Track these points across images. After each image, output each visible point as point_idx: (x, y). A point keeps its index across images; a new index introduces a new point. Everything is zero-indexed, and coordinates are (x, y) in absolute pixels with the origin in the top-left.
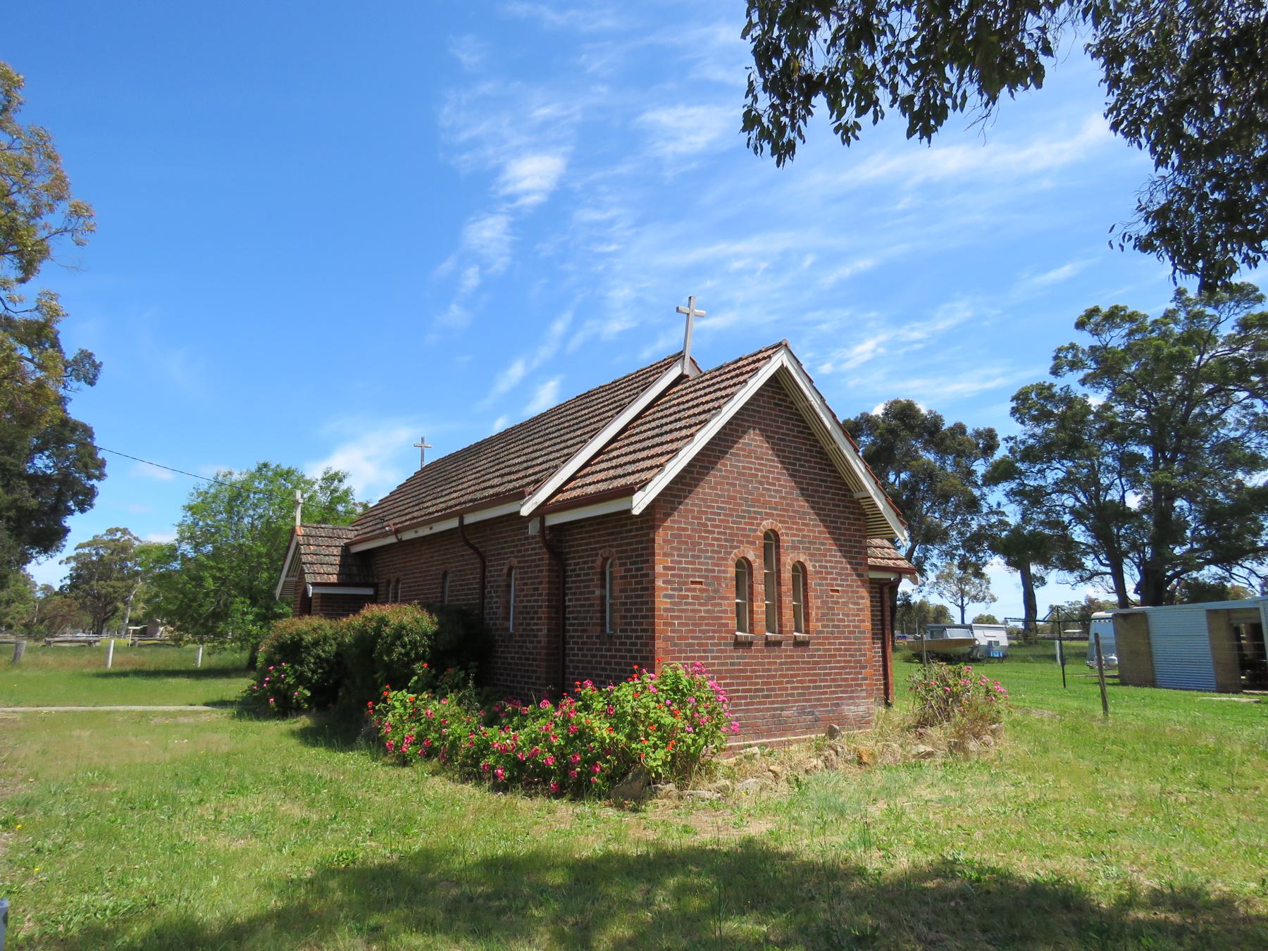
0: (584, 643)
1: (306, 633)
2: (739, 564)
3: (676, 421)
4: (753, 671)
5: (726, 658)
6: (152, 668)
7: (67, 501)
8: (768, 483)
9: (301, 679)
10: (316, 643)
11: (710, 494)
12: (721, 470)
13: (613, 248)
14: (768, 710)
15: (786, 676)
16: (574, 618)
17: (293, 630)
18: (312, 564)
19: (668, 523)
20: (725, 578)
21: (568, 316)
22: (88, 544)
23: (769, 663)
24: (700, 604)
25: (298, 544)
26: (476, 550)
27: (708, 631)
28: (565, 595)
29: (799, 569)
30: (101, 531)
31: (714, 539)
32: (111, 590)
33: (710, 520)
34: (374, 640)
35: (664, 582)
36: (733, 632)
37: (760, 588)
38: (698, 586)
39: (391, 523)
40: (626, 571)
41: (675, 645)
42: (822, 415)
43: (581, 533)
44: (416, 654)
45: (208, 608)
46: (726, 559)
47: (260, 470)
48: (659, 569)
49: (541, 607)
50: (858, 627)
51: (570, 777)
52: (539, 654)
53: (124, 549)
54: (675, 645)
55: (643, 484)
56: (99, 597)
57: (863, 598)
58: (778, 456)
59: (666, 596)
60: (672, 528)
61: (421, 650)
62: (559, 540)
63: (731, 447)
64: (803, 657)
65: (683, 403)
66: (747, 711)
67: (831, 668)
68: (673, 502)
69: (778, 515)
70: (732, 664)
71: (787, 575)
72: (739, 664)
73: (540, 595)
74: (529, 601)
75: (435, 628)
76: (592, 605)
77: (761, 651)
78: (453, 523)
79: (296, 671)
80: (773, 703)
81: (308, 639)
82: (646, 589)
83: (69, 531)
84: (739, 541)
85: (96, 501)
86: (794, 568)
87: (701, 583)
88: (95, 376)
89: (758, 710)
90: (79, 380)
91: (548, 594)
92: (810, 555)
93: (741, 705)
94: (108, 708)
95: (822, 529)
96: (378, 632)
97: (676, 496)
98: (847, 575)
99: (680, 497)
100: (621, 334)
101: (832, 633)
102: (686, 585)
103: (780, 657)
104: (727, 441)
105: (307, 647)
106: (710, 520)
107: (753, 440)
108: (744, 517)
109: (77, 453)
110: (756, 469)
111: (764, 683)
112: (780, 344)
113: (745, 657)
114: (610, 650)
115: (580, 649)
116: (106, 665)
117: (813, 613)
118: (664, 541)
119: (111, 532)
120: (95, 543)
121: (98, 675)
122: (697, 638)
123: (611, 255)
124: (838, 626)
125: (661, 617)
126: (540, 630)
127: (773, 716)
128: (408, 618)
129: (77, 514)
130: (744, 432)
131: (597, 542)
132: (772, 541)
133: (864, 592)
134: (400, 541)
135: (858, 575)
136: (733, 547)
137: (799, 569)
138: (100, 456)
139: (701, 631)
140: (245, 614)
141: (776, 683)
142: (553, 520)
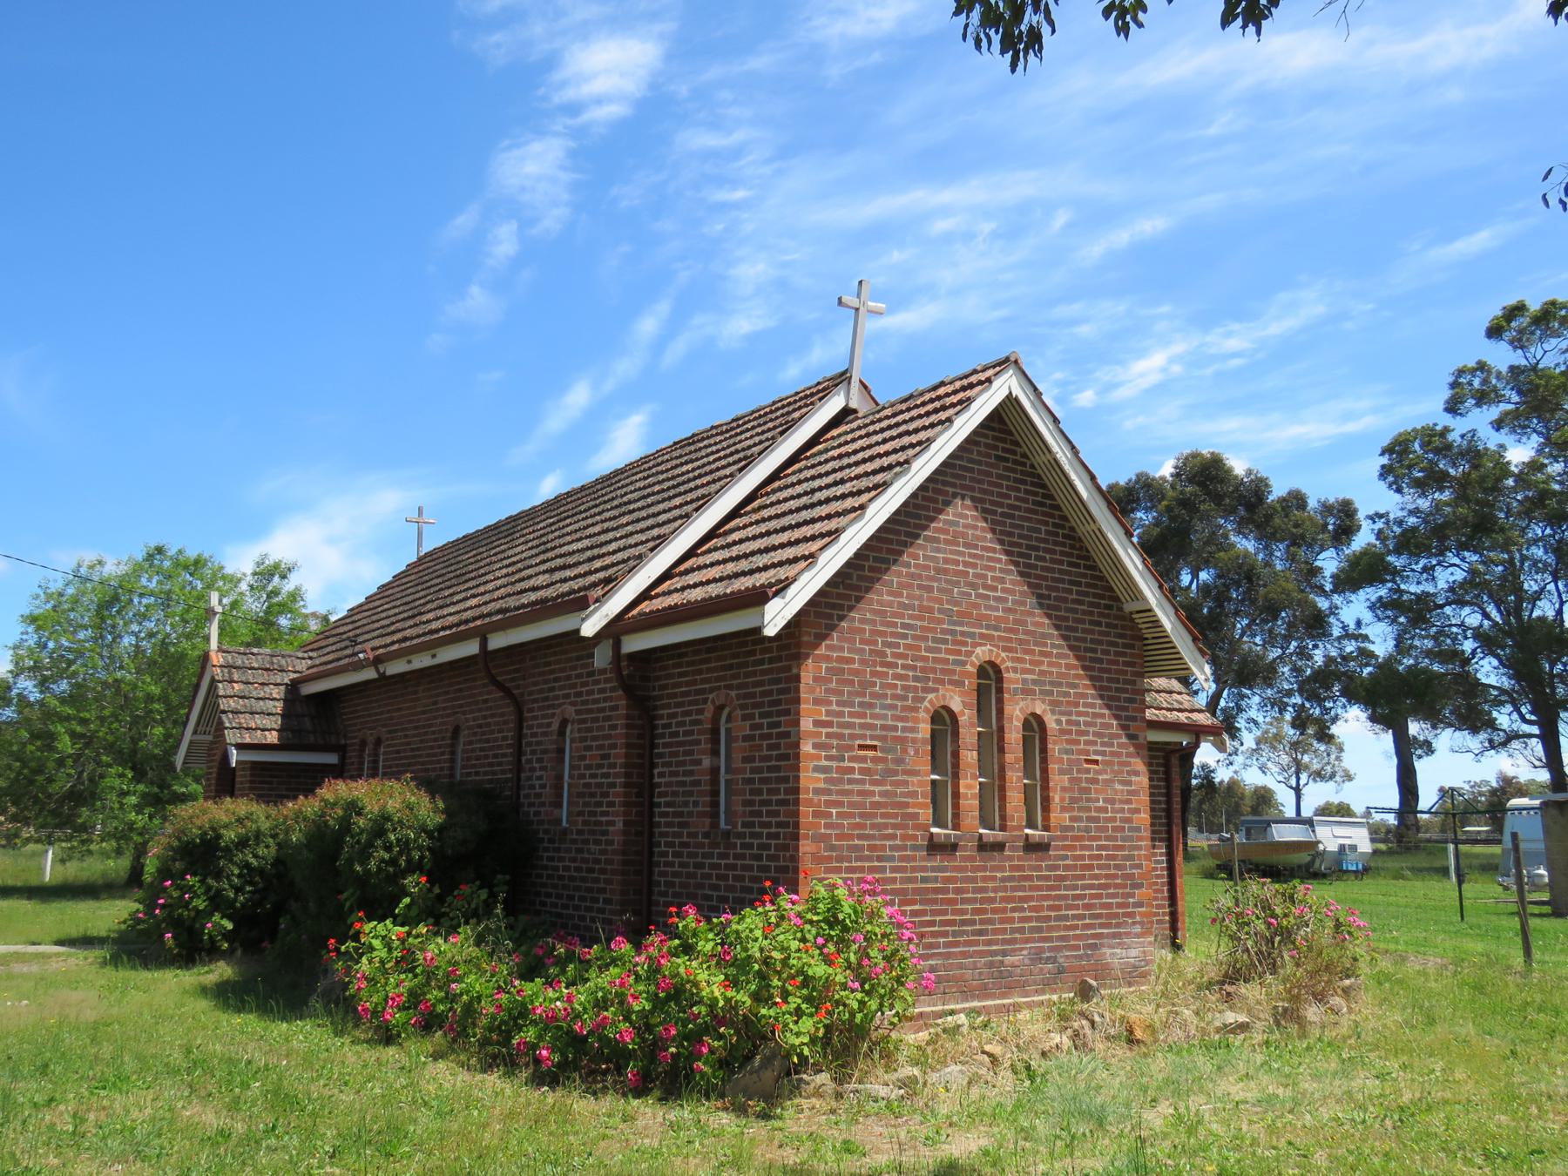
1: (226, 826)
2: (936, 718)
3: (836, 484)
4: (958, 891)
5: (914, 869)
8: (986, 587)
9: (217, 902)
10: (242, 843)
11: (890, 604)
12: (908, 565)
13: (740, 194)
14: (981, 954)
17: (204, 821)
19: (822, 650)
20: (914, 741)
21: (664, 307)
23: (985, 879)
25: (213, 681)
26: (508, 692)
27: (886, 826)
28: (653, 766)
29: (1035, 727)
31: (897, 677)
33: (890, 645)
35: (815, 746)
36: (926, 828)
37: (970, 757)
38: (870, 753)
41: (833, 848)
42: (1073, 476)
43: (679, 665)
44: (409, 861)
46: (916, 709)
47: (150, 557)
48: (806, 724)
49: (613, 785)
54: (833, 848)
57: (1136, 773)
59: (817, 769)
60: (828, 659)
61: (416, 855)
63: (925, 528)
64: (1039, 868)
65: (848, 454)
66: (948, 956)
67: (1084, 887)
68: (830, 617)
70: (924, 880)
71: (1014, 735)
72: (936, 879)
76: (697, 783)
77: (972, 859)
78: (471, 648)
79: (209, 888)
80: (990, 943)
81: (230, 835)
82: (785, 757)
86: (1027, 725)
87: (874, 748)
89: (965, 955)
97: (834, 606)
98: (1113, 736)
99: (841, 607)
100: (754, 338)
101: (1087, 830)
102: (849, 751)
103: (1002, 869)
105: (227, 849)
106: (890, 645)
107: (961, 515)
108: (945, 642)
110: (966, 564)
111: (976, 911)
112: (1007, 360)
113: (945, 869)
117: (1056, 798)
118: (816, 679)
124: (1097, 820)
125: (810, 803)
127: (991, 965)
128: (395, 802)
130: (947, 503)
132: (990, 681)
133: (1139, 765)
135: (1131, 737)
136: (927, 690)
137: (1035, 727)
139: (873, 826)
140: (123, 794)
141: (994, 911)
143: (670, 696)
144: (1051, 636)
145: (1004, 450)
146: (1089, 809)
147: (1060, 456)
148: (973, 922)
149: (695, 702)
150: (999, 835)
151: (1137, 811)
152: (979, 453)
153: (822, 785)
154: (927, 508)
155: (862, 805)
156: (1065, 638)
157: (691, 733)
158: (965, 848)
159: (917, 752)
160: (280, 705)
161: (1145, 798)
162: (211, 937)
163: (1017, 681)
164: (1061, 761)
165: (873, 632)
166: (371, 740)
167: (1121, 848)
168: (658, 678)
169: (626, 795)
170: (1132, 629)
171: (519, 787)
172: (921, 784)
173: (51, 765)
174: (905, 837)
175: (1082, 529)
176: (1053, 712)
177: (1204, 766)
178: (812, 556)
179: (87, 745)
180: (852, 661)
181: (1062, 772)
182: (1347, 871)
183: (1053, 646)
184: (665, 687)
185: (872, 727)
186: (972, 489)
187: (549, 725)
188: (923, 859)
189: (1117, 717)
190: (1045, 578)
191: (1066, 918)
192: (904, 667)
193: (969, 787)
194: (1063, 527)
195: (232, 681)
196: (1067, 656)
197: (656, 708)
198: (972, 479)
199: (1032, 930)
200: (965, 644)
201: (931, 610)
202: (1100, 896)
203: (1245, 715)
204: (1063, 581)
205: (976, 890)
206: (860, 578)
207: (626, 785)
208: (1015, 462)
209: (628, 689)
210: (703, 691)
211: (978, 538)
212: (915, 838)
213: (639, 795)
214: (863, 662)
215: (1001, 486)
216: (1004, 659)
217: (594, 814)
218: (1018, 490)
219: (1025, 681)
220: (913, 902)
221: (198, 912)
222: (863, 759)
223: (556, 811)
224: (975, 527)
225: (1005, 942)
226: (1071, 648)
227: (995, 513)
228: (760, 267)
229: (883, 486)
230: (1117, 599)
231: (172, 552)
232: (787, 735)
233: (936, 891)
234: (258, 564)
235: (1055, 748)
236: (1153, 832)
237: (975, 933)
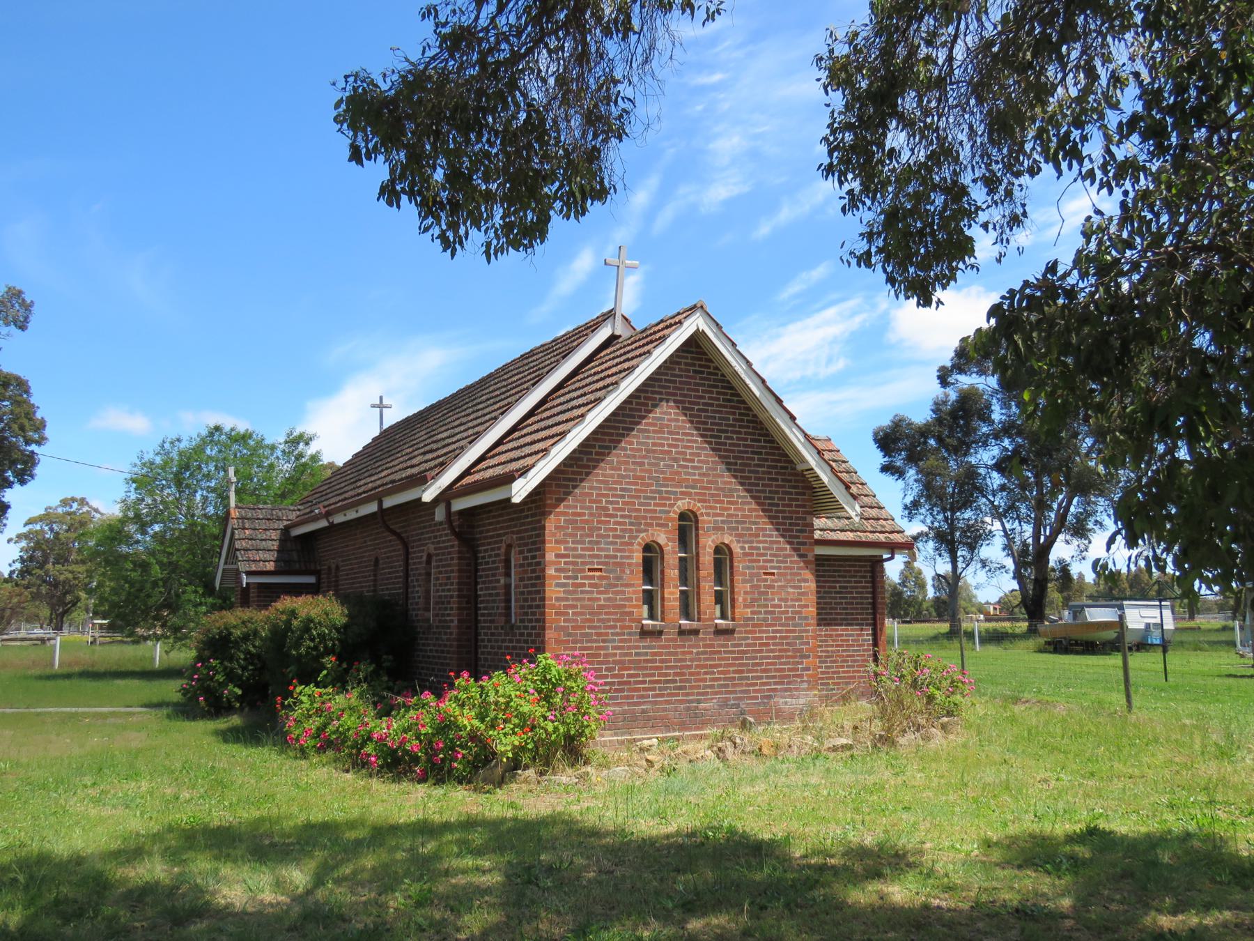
0: (492, 634)
1: (235, 627)
2: (647, 548)
3: (582, 396)
4: (662, 661)
5: (629, 647)
6: (102, 670)
7: (5, 471)
8: (685, 460)
9: (231, 677)
10: (245, 638)
11: (612, 476)
12: (625, 449)
13: (717, 77)
14: (681, 702)
15: (705, 666)
16: (485, 608)
17: (220, 624)
18: (246, 550)
19: (561, 509)
20: (630, 564)
21: (653, 182)
22: (40, 519)
23: (683, 653)
24: (599, 593)
25: (233, 529)
26: (398, 535)
27: (609, 620)
28: (476, 583)
29: (723, 556)
30: (54, 502)
31: (616, 523)
32: (70, 576)
33: (611, 502)
34: (284, 636)
35: (557, 570)
36: (639, 620)
37: (673, 573)
38: (597, 574)
39: (321, 505)
40: (525, 558)
41: (569, 635)
42: (748, 381)
43: (488, 518)
44: (326, 647)
45: (158, 597)
46: (632, 544)
47: (211, 434)
48: (550, 556)
49: (452, 597)
50: (800, 613)
51: (435, 763)
52: (451, 646)
53: (83, 524)
54: (569, 635)
55: (524, 471)
56: (55, 584)
57: (806, 581)
58: (697, 429)
59: (558, 585)
60: (565, 514)
61: (330, 644)
62: (468, 527)
63: (639, 423)
64: (727, 646)
65: (598, 373)
66: (655, 703)
67: (762, 658)
68: (567, 487)
69: (697, 494)
70: (637, 654)
71: (707, 558)
72: (646, 654)
73: (452, 584)
74: (443, 591)
75: (344, 620)
76: (498, 595)
77: (674, 640)
78: (372, 508)
79: (226, 668)
80: (687, 694)
81: (237, 633)
82: (538, 578)
83: (9, 507)
84: (646, 524)
85: (38, 470)
86: (718, 550)
87: (600, 570)
88: (26, 318)
89: (668, 702)
90: (7, 324)
91: (459, 584)
92: (737, 535)
93: (648, 696)
94: (39, 710)
95: (754, 506)
96: (288, 623)
97: (569, 480)
98: (786, 556)
99: (575, 480)
100: (729, 203)
101: (765, 619)
102: (580, 572)
103: (698, 646)
104: (633, 416)
105: (236, 642)
106: (611, 502)
107: (666, 413)
108: (654, 498)
109: (12, 412)
110: (669, 445)
111: (676, 674)
112: (695, 306)
113: (654, 647)
114: (511, 641)
115: (489, 641)
116: (53, 665)
117: (740, 599)
118: (557, 528)
119: (65, 502)
120: (48, 517)
121: (40, 678)
122: (595, 628)
123: (715, 88)
124: (772, 613)
125: (553, 606)
126: (452, 621)
127: (688, 709)
128: (324, 610)
129: (17, 486)
130: (655, 406)
131: (502, 528)
132: (687, 527)
133: (808, 575)
134: (332, 526)
135: (800, 556)
136: (639, 531)
137: (723, 556)
138: (39, 415)
139: (599, 620)
140: (197, 605)
141: (691, 674)
142: (459, 505)
143: (486, 538)
144: (737, 490)
145: (700, 366)
146: (766, 606)
147: (738, 368)
148: (675, 681)
149: (496, 542)
150: (695, 624)
151: (807, 606)
152: (680, 370)
153: (562, 595)
154: (640, 410)
155: (591, 607)
156: (747, 491)
157: (494, 562)
158: (668, 633)
159: (632, 572)
160: (276, 544)
161: (813, 597)
162: (228, 700)
163: (709, 522)
164: (745, 574)
165: (598, 495)
166: (333, 566)
167: (794, 631)
168: (479, 526)
169: (459, 603)
170: (803, 481)
171: (407, 598)
172: (635, 592)
173: (148, 586)
174: (622, 627)
175: (761, 416)
176: (738, 542)
177: (1061, 561)
178: (546, 450)
179: (173, 571)
180: (584, 514)
181: (745, 581)
182: (1152, 645)
183: (739, 497)
184: (481, 532)
185: (598, 556)
186: (675, 395)
187: (499, 548)
188: (636, 641)
189: (789, 543)
190: (733, 451)
191: (747, 678)
192: (622, 516)
193: (671, 593)
194: (748, 415)
195: (244, 528)
196: (750, 503)
197: (478, 546)
198: (674, 388)
199: (721, 686)
200: (669, 499)
201: (643, 478)
202: (775, 664)
203: (1092, 519)
204: (746, 452)
205: (676, 661)
206: (589, 460)
207: (459, 596)
208: (709, 373)
209: (458, 535)
210: (499, 535)
211: (679, 427)
212: (631, 627)
213: (467, 603)
214: (591, 515)
215: (698, 391)
216: (699, 507)
217: (443, 615)
218: (712, 392)
219: (716, 522)
220: (630, 669)
221: (220, 684)
222: (592, 578)
223: (426, 614)
224: (677, 420)
225: (699, 694)
226: (752, 497)
227: (693, 409)
228: (736, 140)
229: (598, 401)
230: (792, 462)
231: (227, 428)
232: (539, 564)
233: (647, 661)
234: (288, 435)
235: (739, 566)
236: (819, 620)
237: (676, 688)
